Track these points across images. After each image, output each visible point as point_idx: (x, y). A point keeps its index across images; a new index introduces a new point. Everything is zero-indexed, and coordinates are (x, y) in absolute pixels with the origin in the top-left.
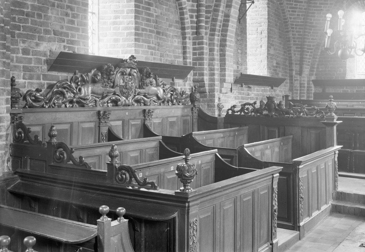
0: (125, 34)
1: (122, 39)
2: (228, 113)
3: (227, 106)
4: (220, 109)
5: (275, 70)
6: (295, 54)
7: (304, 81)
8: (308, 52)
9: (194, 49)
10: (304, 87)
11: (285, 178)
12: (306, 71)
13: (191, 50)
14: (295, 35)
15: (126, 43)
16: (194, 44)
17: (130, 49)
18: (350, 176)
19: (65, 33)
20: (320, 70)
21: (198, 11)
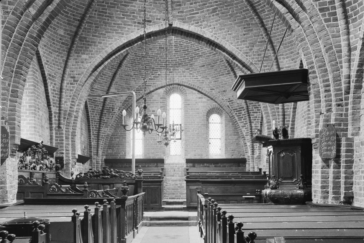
0: (28, 127)
1: (26, 130)
2: (77, 177)
3: (76, 173)
4: (72, 175)
5: (84, 152)
6: (93, 141)
7: (99, 159)
8: (101, 140)
9: (56, 137)
10: (99, 164)
11: (185, 207)
12: (100, 152)
13: (320, 174)
14: (94, 128)
15: (29, 133)
16: (56, 134)
17: (32, 136)
18: (178, 208)
19: (28, 131)
20: (109, 152)
21: (60, 113)
